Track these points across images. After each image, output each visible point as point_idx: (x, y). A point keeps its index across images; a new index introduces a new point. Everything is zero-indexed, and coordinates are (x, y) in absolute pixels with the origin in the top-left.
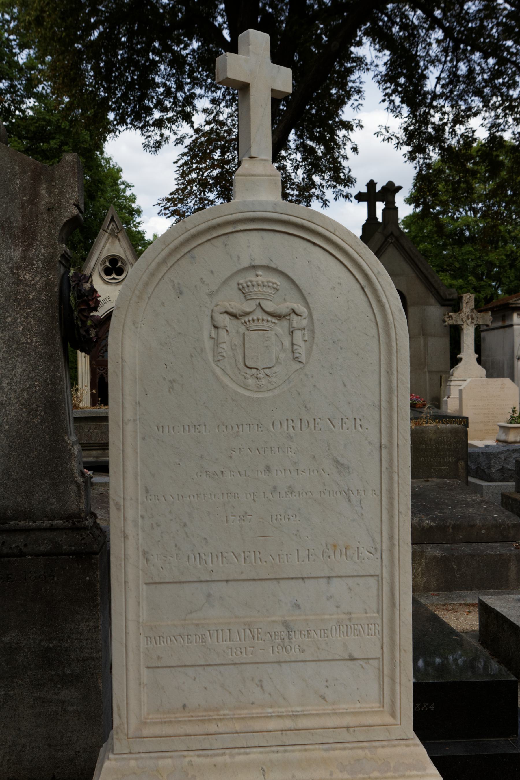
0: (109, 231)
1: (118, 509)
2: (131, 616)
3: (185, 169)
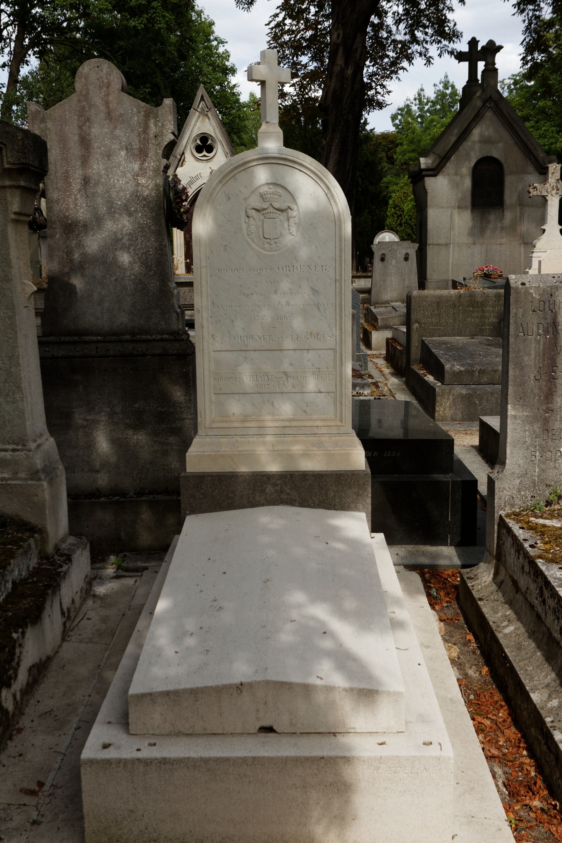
0: (199, 110)
1: (199, 312)
2: (206, 366)
3: (277, 31)
